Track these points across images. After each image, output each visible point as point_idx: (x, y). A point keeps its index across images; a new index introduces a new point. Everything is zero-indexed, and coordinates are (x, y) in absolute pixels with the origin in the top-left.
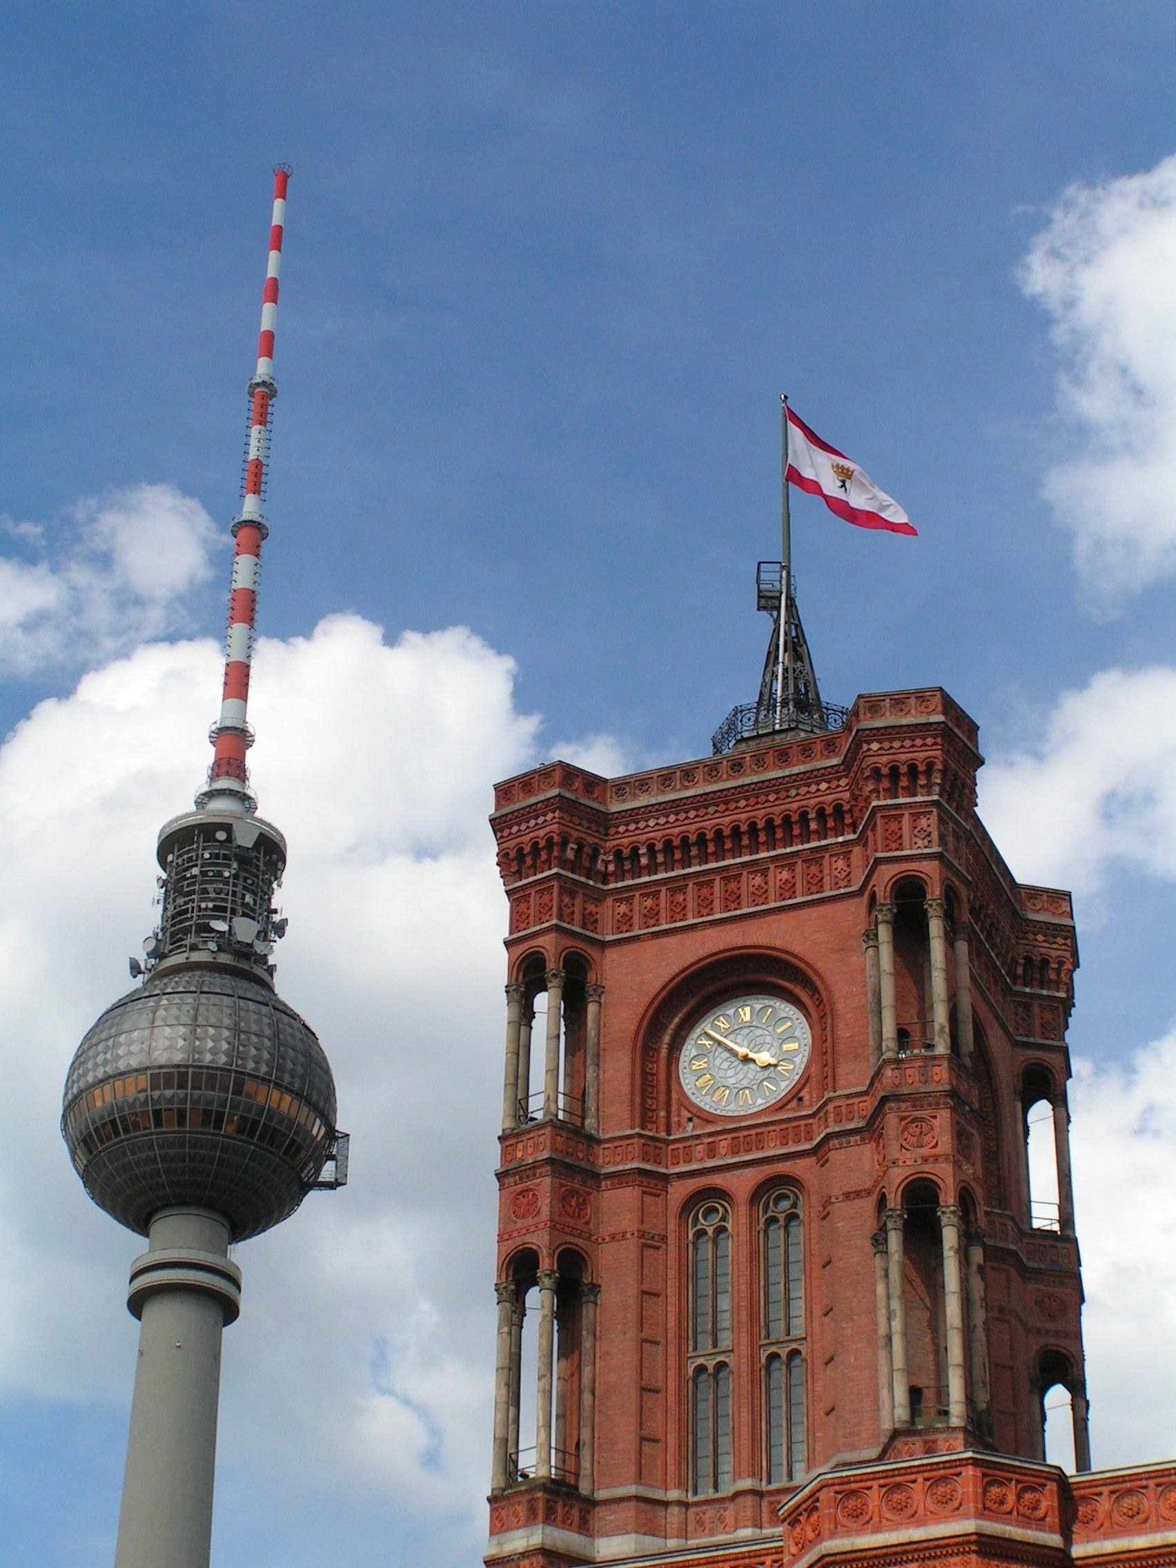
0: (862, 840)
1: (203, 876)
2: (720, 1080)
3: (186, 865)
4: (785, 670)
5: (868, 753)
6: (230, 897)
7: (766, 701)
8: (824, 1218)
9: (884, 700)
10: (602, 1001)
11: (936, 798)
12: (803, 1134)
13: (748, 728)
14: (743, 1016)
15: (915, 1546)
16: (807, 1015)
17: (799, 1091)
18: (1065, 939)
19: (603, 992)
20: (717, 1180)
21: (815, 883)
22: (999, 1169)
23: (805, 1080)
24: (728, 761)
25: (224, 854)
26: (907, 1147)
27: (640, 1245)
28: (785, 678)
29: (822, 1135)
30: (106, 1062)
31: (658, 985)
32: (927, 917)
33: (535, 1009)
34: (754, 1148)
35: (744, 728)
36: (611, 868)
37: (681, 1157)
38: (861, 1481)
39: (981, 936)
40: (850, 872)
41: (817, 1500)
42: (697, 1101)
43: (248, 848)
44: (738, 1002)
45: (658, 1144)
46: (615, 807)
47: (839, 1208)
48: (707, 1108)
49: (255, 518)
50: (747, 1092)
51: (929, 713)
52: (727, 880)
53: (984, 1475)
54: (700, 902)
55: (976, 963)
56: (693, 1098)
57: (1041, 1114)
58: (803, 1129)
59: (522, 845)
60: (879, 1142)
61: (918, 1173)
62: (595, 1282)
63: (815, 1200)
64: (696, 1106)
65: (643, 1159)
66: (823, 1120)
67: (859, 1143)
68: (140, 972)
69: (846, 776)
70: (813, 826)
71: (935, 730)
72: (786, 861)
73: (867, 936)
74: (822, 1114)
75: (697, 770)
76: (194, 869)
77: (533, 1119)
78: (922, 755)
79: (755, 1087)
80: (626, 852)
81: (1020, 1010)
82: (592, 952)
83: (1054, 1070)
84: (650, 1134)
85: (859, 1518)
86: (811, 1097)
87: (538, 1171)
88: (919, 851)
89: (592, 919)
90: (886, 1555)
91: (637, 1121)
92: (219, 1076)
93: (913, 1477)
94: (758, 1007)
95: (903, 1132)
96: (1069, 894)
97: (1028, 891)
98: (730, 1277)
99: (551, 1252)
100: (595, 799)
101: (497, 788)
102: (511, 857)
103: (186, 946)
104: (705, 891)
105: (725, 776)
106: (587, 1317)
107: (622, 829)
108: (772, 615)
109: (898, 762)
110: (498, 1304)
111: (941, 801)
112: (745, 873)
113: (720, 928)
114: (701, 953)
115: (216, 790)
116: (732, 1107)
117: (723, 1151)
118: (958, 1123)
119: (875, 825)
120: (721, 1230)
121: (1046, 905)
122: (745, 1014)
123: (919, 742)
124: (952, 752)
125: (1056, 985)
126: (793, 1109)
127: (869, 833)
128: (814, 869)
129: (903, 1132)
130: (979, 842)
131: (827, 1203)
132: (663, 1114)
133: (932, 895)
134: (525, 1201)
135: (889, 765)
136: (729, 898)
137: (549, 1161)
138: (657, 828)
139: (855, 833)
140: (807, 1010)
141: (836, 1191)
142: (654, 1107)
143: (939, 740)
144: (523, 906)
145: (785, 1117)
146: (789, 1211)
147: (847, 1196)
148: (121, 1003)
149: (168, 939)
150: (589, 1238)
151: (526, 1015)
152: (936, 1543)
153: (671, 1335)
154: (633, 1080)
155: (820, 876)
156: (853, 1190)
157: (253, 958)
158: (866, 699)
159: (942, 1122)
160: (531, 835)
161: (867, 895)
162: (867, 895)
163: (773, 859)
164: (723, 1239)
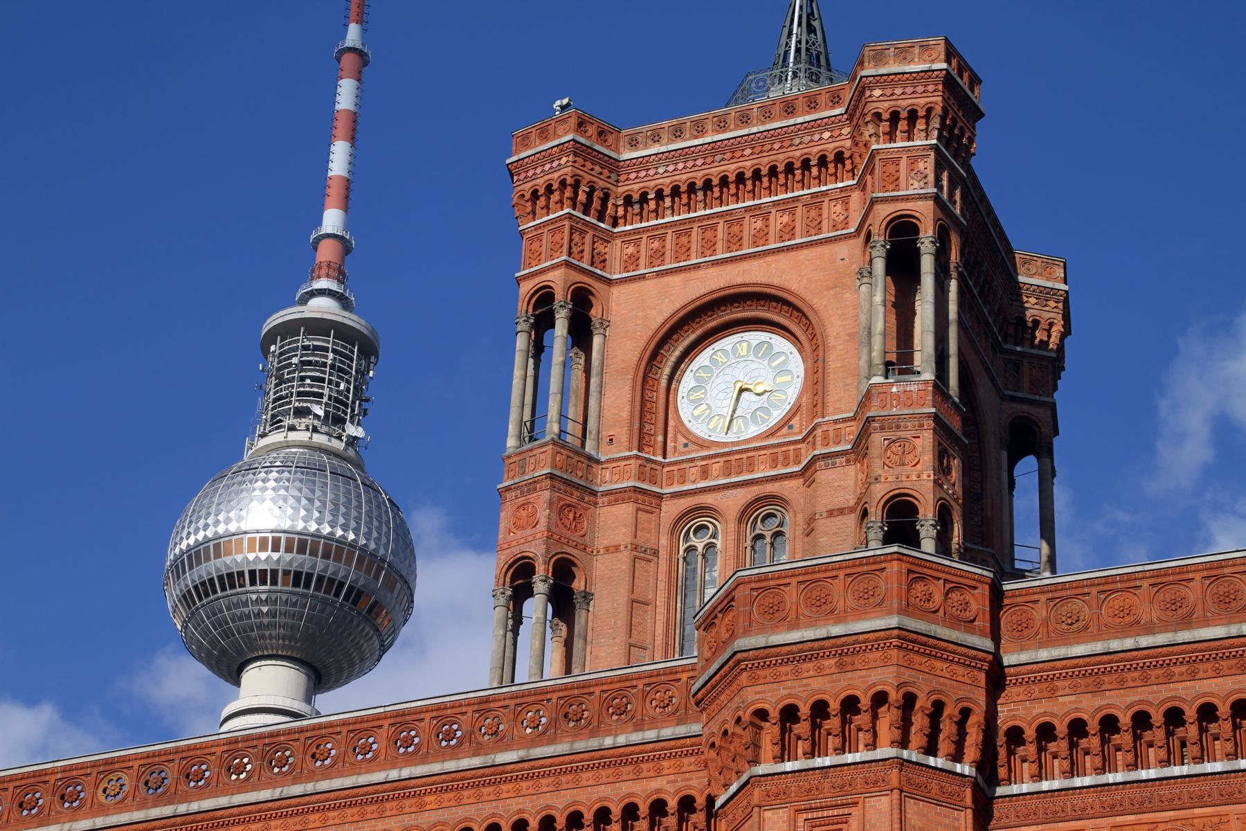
0: (861, 185)
5: (870, 99)
8: (808, 535)
10: (607, 334)
11: (934, 141)
12: (791, 458)
14: (740, 351)
17: (790, 419)
19: (608, 326)
20: (708, 499)
21: (813, 226)
23: (795, 410)
26: (890, 465)
27: (632, 558)
29: (809, 458)
31: (660, 320)
36: (621, 212)
37: (676, 478)
39: (970, 282)
40: (847, 217)
41: (733, 599)
45: (653, 466)
46: (627, 155)
47: (824, 525)
49: (358, 45)
50: (741, 420)
51: (932, 62)
52: (730, 224)
53: (909, 571)
54: (704, 244)
57: (1027, 468)
58: (791, 453)
62: (587, 590)
63: (800, 519)
64: (695, 436)
67: (844, 464)
72: (787, 206)
73: (861, 274)
74: (810, 439)
75: (706, 121)
78: (922, 101)
79: (748, 416)
82: (597, 286)
83: (1040, 424)
84: (647, 456)
85: (776, 615)
86: (801, 425)
87: (538, 486)
88: (915, 192)
89: (601, 259)
91: (635, 443)
92: (309, 542)
93: (834, 573)
94: (754, 343)
95: (886, 450)
97: (1023, 256)
99: (547, 560)
100: (608, 147)
102: (526, 198)
103: (284, 427)
104: (709, 234)
105: (732, 127)
106: (580, 622)
107: (633, 176)
111: (940, 145)
115: (316, 290)
117: (715, 473)
118: (940, 444)
119: (873, 168)
120: (710, 546)
121: (1040, 271)
122: (742, 349)
126: (784, 436)
129: (886, 450)
130: (976, 199)
131: (811, 520)
132: (660, 438)
133: (926, 232)
134: (524, 513)
135: (890, 111)
136: (731, 240)
137: (551, 476)
138: (666, 175)
141: (821, 508)
142: (652, 432)
145: (777, 442)
147: (831, 513)
150: (585, 549)
153: (659, 640)
154: (632, 406)
159: (925, 441)
160: (546, 178)
163: (775, 203)
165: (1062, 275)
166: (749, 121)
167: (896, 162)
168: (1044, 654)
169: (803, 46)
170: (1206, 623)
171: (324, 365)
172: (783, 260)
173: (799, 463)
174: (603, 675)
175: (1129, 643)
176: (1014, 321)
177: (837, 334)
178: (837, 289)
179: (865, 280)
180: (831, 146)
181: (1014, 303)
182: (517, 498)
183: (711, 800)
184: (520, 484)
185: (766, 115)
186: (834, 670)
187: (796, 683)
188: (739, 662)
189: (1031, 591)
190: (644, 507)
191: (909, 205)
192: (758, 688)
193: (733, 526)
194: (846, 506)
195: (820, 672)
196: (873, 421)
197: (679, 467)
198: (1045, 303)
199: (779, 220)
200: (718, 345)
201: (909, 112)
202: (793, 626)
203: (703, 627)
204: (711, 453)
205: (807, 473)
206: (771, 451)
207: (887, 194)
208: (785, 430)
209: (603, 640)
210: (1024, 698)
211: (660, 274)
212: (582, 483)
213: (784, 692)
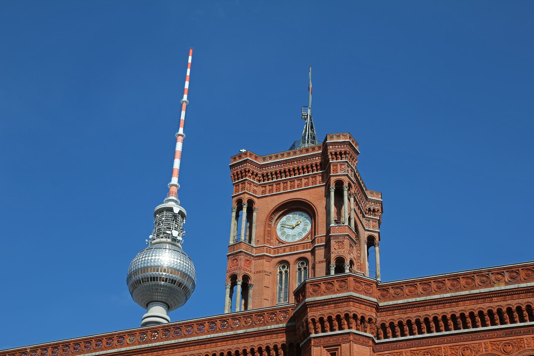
5: (329, 149)
6: (172, 225)
12: (308, 247)
20: (286, 258)
22: (360, 261)
23: (311, 233)
31: (272, 208)
47: (317, 266)
80: (265, 174)
84: (268, 246)
85: (316, 292)
90: (324, 302)
103: (160, 237)
113: (288, 194)
123: (342, 146)
126: (306, 240)
128: (314, 179)
130: (358, 176)
138: (273, 168)
139: (325, 170)
142: (269, 239)
143: (348, 146)
147: (319, 262)
152: (339, 298)
160: (240, 169)
163: (303, 176)
165: (381, 197)
169: (310, 134)
170: (434, 294)
175: (414, 300)
178: (321, 200)
179: (328, 197)
183: (298, 344)
187: (323, 311)
191: (340, 177)
192: (312, 313)
195: (329, 308)
197: (277, 249)
199: (304, 181)
202: (322, 295)
203: (296, 295)
207: (334, 174)
212: (250, 253)
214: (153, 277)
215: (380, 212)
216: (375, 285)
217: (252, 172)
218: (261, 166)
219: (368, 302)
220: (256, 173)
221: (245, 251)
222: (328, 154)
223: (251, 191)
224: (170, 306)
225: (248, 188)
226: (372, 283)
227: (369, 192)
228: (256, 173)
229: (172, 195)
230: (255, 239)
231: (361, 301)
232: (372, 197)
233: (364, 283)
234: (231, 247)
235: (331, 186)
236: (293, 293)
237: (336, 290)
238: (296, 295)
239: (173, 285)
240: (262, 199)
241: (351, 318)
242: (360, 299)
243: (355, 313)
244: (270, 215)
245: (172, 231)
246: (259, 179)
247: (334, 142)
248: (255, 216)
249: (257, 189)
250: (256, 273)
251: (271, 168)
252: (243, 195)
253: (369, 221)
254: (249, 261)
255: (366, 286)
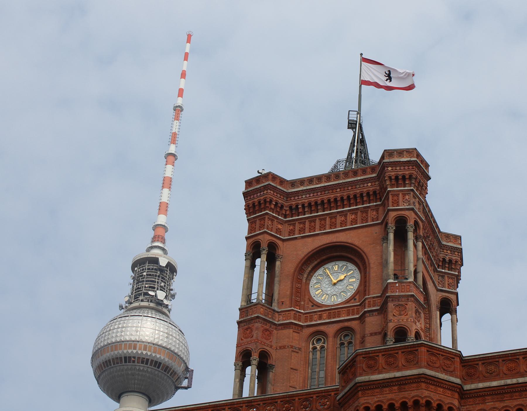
1: (147, 276)
2: (325, 292)
3: (141, 272)
4: (357, 149)
5: (387, 171)
7: (349, 159)
8: (362, 343)
9: (394, 152)
12: (355, 312)
13: (342, 168)
14: (335, 268)
15: (396, 379)
16: (359, 269)
17: (355, 296)
18: (458, 253)
19: (282, 257)
20: (322, 328)
22: (430, 335)
23: (357, 292)
24: (334, 175)
25: (155, 268)
28: (357, 152)
29: (363, 312)
30: (108, 338)
31: (303, 255)
32: (407, 231)
33: (256, 264)
34: (336, 317)
35: (341, 168)
36: (288, 213)
38: (374, 353)
42: (316, 299)
43: (164, 267)
44: (333, 263)
45: (300, 314)
48: (319, 302)
49: (173, 152)
52: (331, 218)
55: (424, 257)
56: (314, 298)
58: (355, 310)
59: (254, 202)
60: (385, 314)
61: (399, 325)
63: (358, 336)
65: (294, 319)
66: (363, 306)
67: (377, 315)
68: (123, 309)
69: (378, 181)
70: (365, 199)
71: (413, 163)
73: (383, 239)
74: (363, 304)
76: (144, 273)
77: (252, 302)
80: (294, 207)
81: (440, 278)
84: (297, 310)
85: (373, 368)
88: (405, 207)
94: (340, 265)
96: (460, 237)
97: (444, 234)
98: (325, 365)
101: (246, 182)
107: (292, 198)
108: (353, 131)
109: (399, 174)
110: (235, 370)
111: (414, 189)
112: (338, 216)
114: (320, 244)
115: (154, 246)
116: (328, 302)
117: (325, 318)
120: (322, 347)
122: (335, 268)
123: (406, 168)
124: (419, 173)
125: (455, 270)
126: (352, 303)
127: (386, 201)
128: (364, 215)
130: (427, 211)
131: (363, 337)
133: (410, 223)
138: (306, 198)
139: (380, 202)
140: (359, 266)
142: (299, 300)
143: (414, 167)
144: (253, 225)
146: (349, 341)
147: (371, 334)
148: (115, 318)
149: (133, 297)
151: (253, 266)
155: (367, 217)
156: (374, 332)
157: (163, 306)
158: (387, 152)
160: (258, 199)
161: (384, 224)
162: (384, 224)
163: (349, 210)
164: (323, 351)
166: (339, 178)
167: (398, 195)
168: (481, 385)
169: (359, 151)
171: (156, 276)
172: (352, 233)
173: (359, 314)
174: (299, 392)
175: (514, 381)
176: (442, 260)
177: (374, 262)
178: (374, 245)
179: (385, 241)
180: (371, 189)
181: (442, 253)
182: (244, 326)
184: (246, 320)
185: (346, 176)
186: (396, 391)
188: (358, 387)
189: (475, 360)
190: (295, 330)
191: (403, 212)
192: (366, 398)
193: (332, 339)
194: (378, 332)
196: (389, 297)
198: (454, 253)
199: (350, 217)
200: (326, 266)
201: (402, 176)
202: (380, 373)
203: (342, 373)
204: (323, 309)
205: (362, 319)
206: (348, 309)
208: (353, 301)
209: (279, 384)
210: (472, 403)
211: (303, 237)
212: (271, 320)
213: (376, 399)
214: (128, 357)
215: (460, 264)
216: (458, 360)
217: (274, 203)
218: (288, 195)
219: (447, 383)
220: (281, 205)
221: (264, 317)
222: (386, 179)
223: (273, 230)
224: (152, 399)
225: (269, 226)
226: (453, 356)
227: (443, 236)
228: (281, 205)
229: (158, 241)
230: (278, 300)
231: (438, 382)
232: (448, 242)
233: (442, 355)
234: (243, 310)
235: (390, 225)
236: (338, 369)
237: (400, 365)
238: (342, 373)
239: (156, 368)
240: (289, 242)
241: (423, 406)
242: (436, 380)
243: (428, 399)
244: (300, 265)
245: (157, 291)
246: (286, 212)
247: (394, 162)
248: (278, 266)
249: (282, 228)
250: (278, 348)
251: (302, 198)
252: (261, 236)
253: (443, 277)
254: (269, 331)
255: (445, 361)
